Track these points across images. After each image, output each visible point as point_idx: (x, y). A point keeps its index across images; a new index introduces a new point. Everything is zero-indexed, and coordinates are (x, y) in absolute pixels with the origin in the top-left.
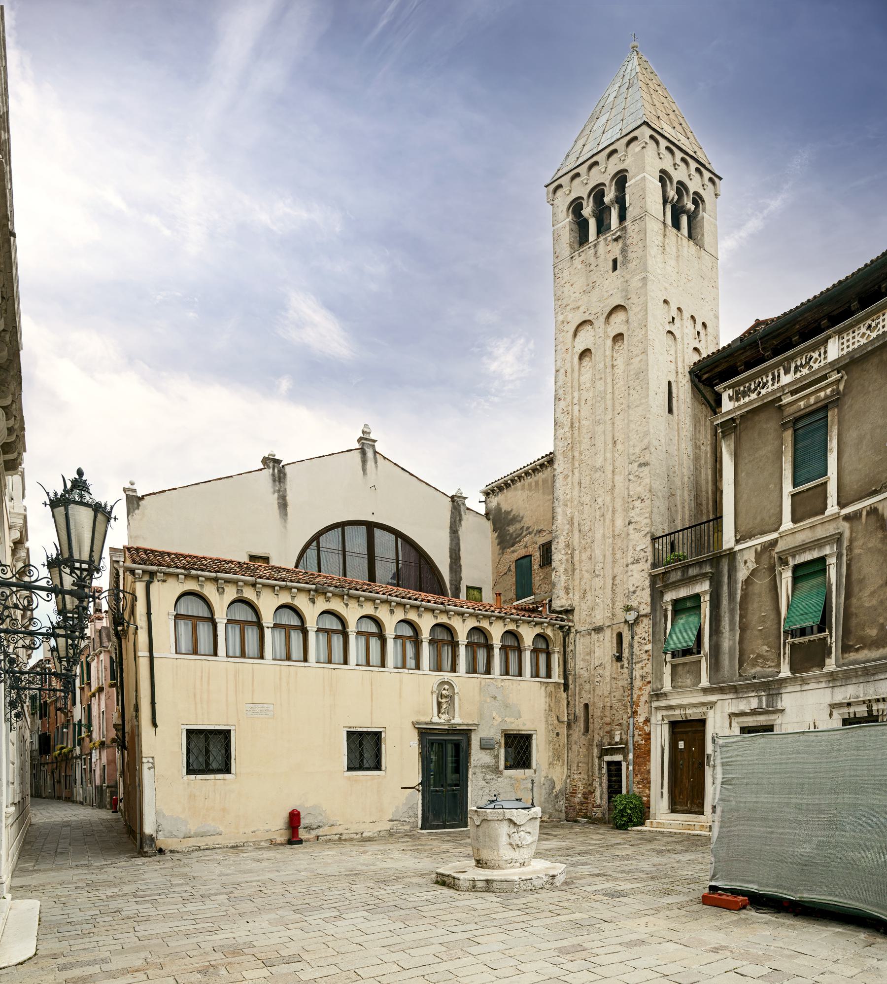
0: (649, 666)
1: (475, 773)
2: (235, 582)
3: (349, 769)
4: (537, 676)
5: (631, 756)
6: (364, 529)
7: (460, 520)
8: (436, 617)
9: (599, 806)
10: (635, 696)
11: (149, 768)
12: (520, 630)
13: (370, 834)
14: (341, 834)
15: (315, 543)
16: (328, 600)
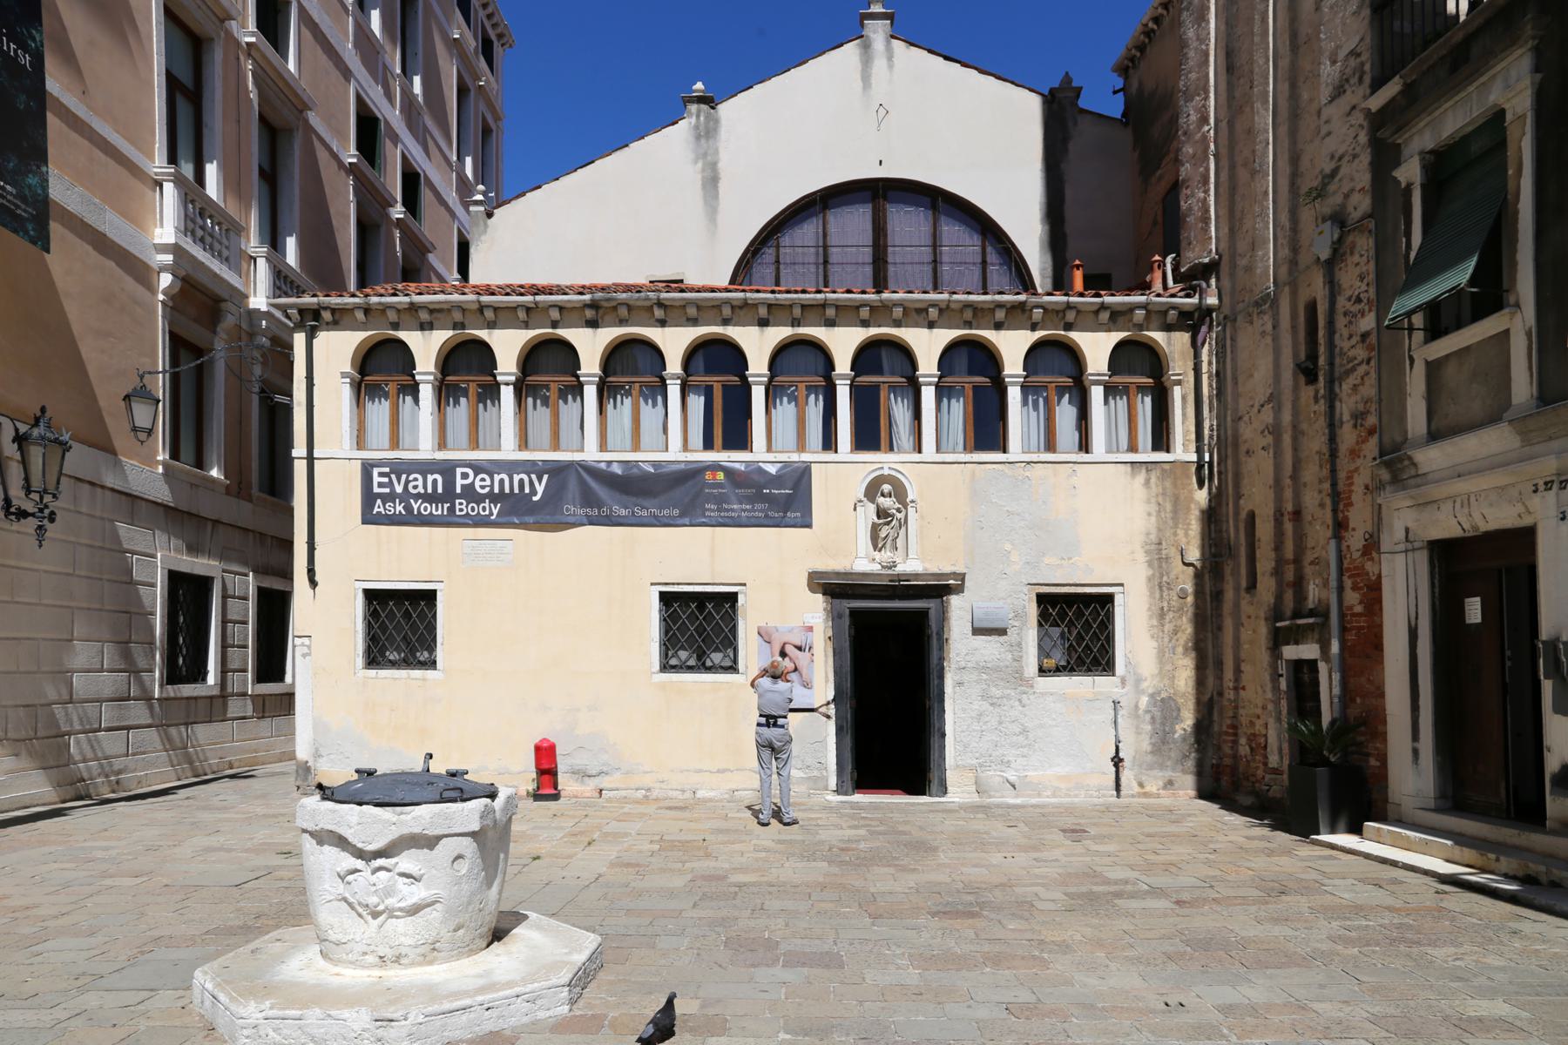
0: (1372, 379)
1: (960, 684)
4: (1133, 448)
5: (1335, 647)
9: (1276, 771)
10: (1342, 475)
11: (304, 656)
13: (711, 794)
14: (649, 790)
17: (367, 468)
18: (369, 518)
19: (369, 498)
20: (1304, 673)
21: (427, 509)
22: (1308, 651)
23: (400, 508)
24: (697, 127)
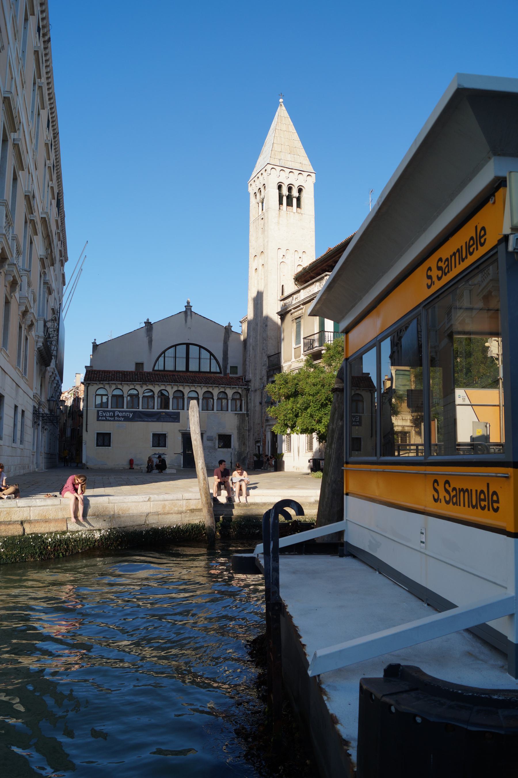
2: (115, 384)
3: (153, 446)
6: (185, 346)
7: (229, 337)
8: (190, 388)
12: (226, 391)
15: (163, 355)
16: (147, 386)
17: (98, 411)
18: (98, 420)
19: (98, 416)
20: (259, 447)
21: (110, 418)
22: (259, 444)
23: (104, 418)
24: (147, 329)
